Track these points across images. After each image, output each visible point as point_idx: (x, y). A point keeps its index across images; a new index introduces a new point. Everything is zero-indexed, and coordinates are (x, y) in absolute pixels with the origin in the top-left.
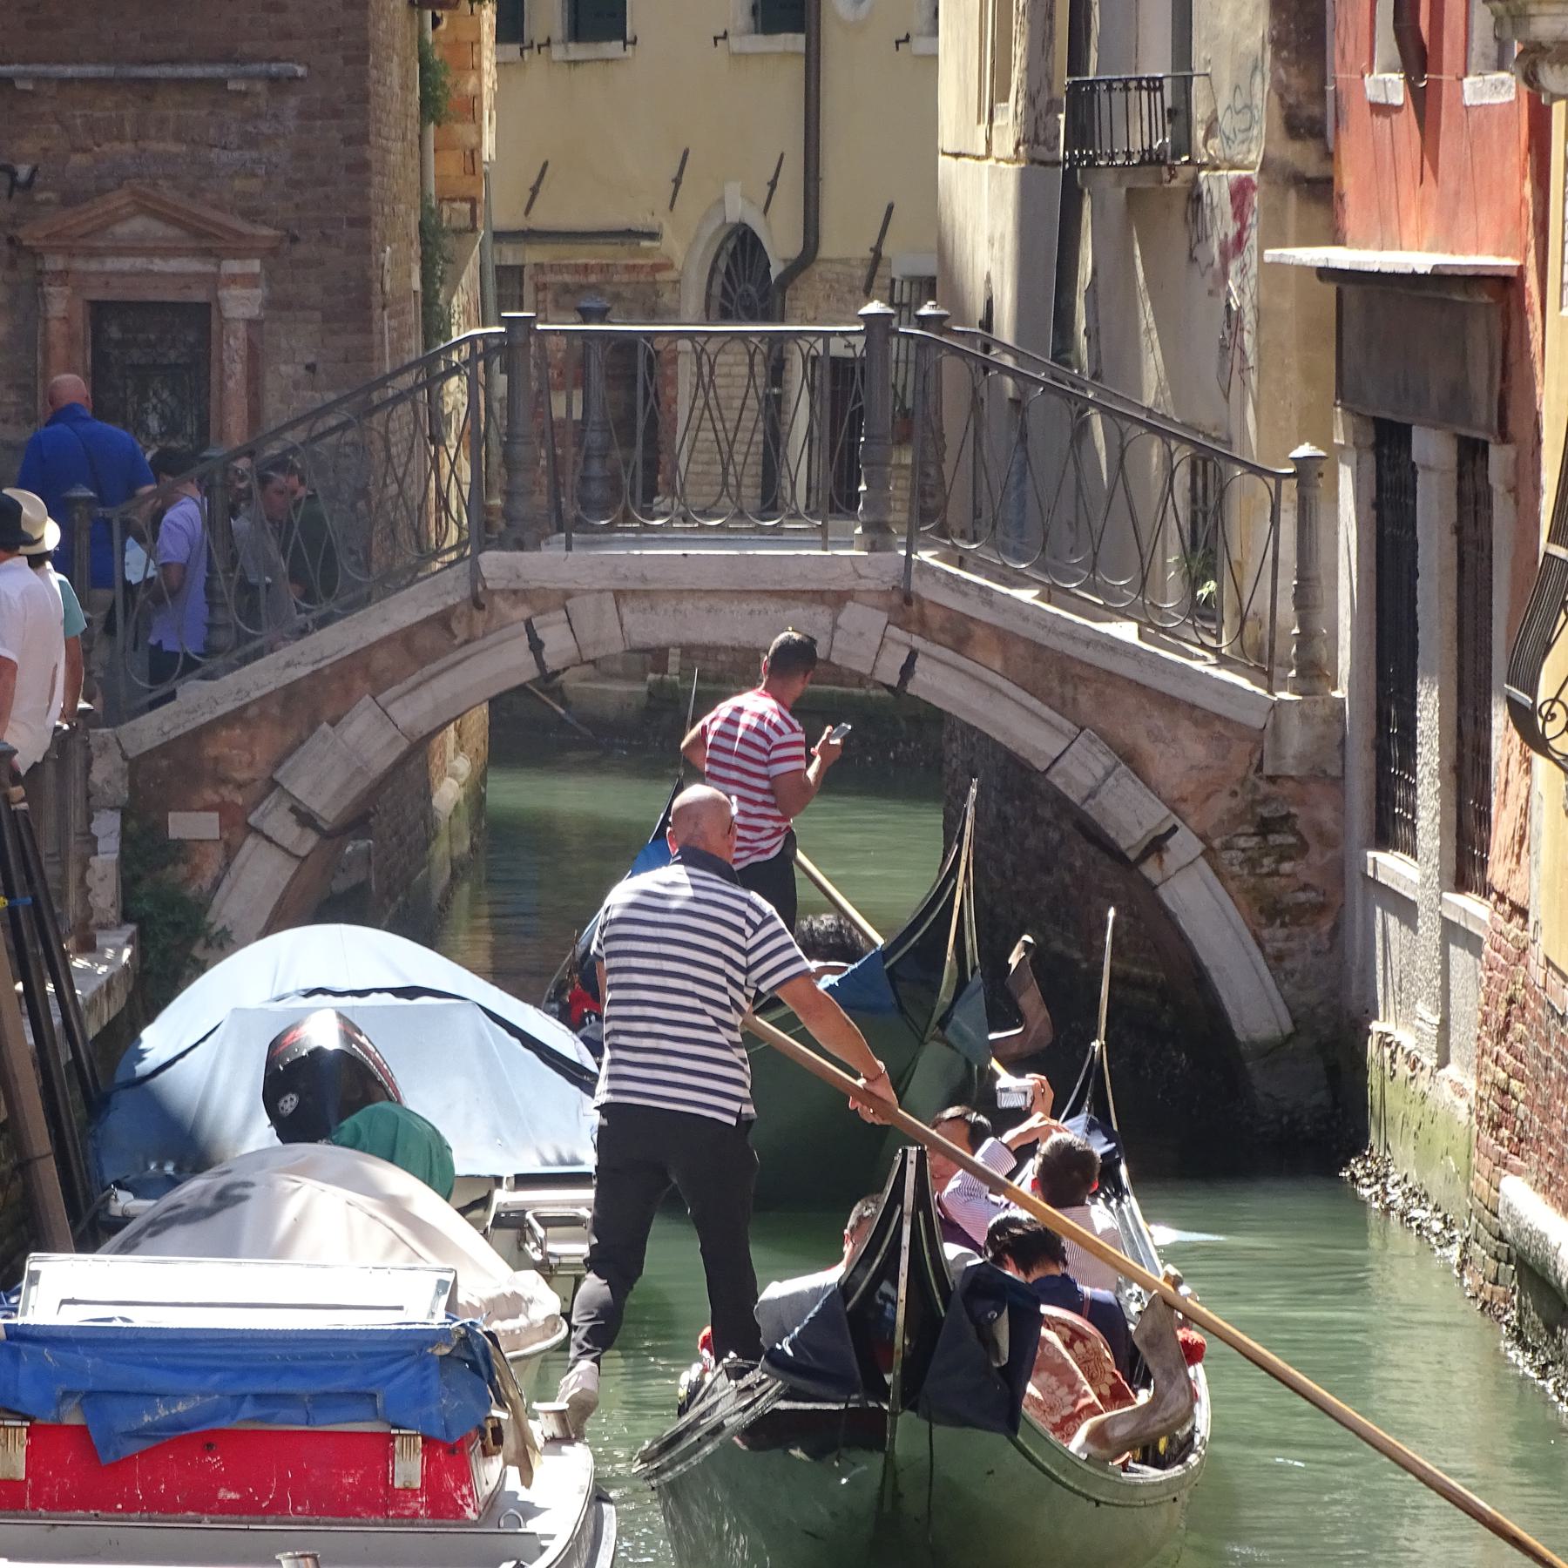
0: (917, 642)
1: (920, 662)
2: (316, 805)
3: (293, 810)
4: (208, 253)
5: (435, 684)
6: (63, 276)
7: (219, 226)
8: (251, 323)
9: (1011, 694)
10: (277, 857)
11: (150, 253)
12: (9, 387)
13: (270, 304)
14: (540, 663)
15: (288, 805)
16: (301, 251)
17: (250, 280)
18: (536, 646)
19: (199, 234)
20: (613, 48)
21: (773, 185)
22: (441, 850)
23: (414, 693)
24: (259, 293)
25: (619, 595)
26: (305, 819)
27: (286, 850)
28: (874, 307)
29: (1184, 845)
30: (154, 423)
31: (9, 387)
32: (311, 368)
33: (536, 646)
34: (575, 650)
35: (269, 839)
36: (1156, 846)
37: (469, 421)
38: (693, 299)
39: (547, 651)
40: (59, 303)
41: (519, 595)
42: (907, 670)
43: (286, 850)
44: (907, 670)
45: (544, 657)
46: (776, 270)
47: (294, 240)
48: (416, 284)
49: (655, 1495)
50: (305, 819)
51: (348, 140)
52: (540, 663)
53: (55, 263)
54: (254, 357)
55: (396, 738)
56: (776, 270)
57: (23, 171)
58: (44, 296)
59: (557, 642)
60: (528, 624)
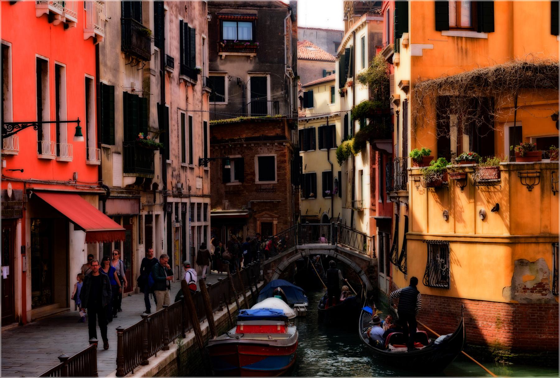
0: (337, 253)
1: (338, 255)
2: (281, 269)
4: (272, 218)
6: (258, 220)
8: (276, 224)
9: (179, 124)
10: (278, 274)
11: (267, 218)
13: (278, 222)
16: (281, 217)
17: (276, 220)
18: (302, 254)
19: (271, 216)
20: (313, 108)
21: (329, 211)
22: (296, 265)
24: (277, 221)
25: (310, 249)
26: (280, 270)
28: (338, 222)
29: (363, 272)
30: (267, 234)
32: (282, 228)
33: (302, 254)
36: (360, 272)
37: (45, 318)
38: (321, 221)
39: (303, 254)
40: (258, 223)
41: (300, 249)
42: (337, 256)
44: (337, 256)
46: (329, 219)
47: (280, 216)
48: (293, 220)
49: (303, 110)
50: (280, 270)
51: (285, 207)
53: (258, 219)
54: (277, 227)
56: (329, 219)
57: (255, 210)
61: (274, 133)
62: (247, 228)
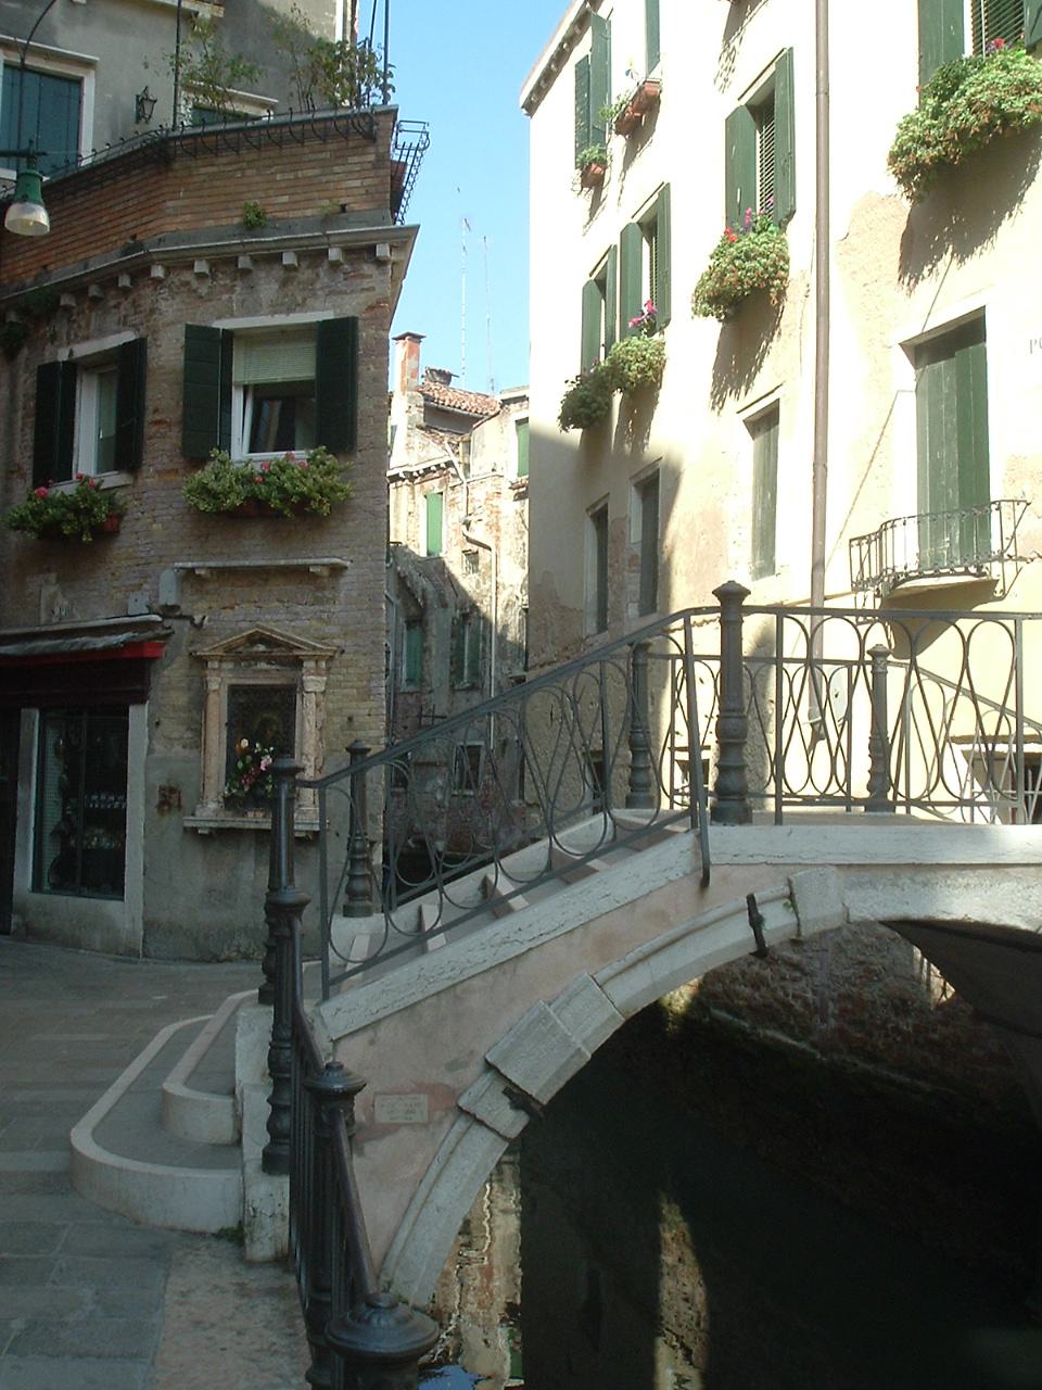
2: (533, 1092)
3: (507, 1092)
5: (653, 961)
7: (302, 643)
12: (188, 729)
14: (759, 937)
15: (502, 1088)
18: (756, 922)
23: (632, 971)
26: (519, 1098)
27: (498, 1133)
31: (188, 729)
33: (756, 922)
34: (794, 928)
35: (481, 1123)
43: (498, 1133)
45: (764, 932)
50: (519, 1098)
52: (759, 937)
55: (613, 1017)
57: (197, 619)
58: (207, 682)
59: (777, 920)
60: (751, 899)
61: (326, 202)
62: (151, 716)
